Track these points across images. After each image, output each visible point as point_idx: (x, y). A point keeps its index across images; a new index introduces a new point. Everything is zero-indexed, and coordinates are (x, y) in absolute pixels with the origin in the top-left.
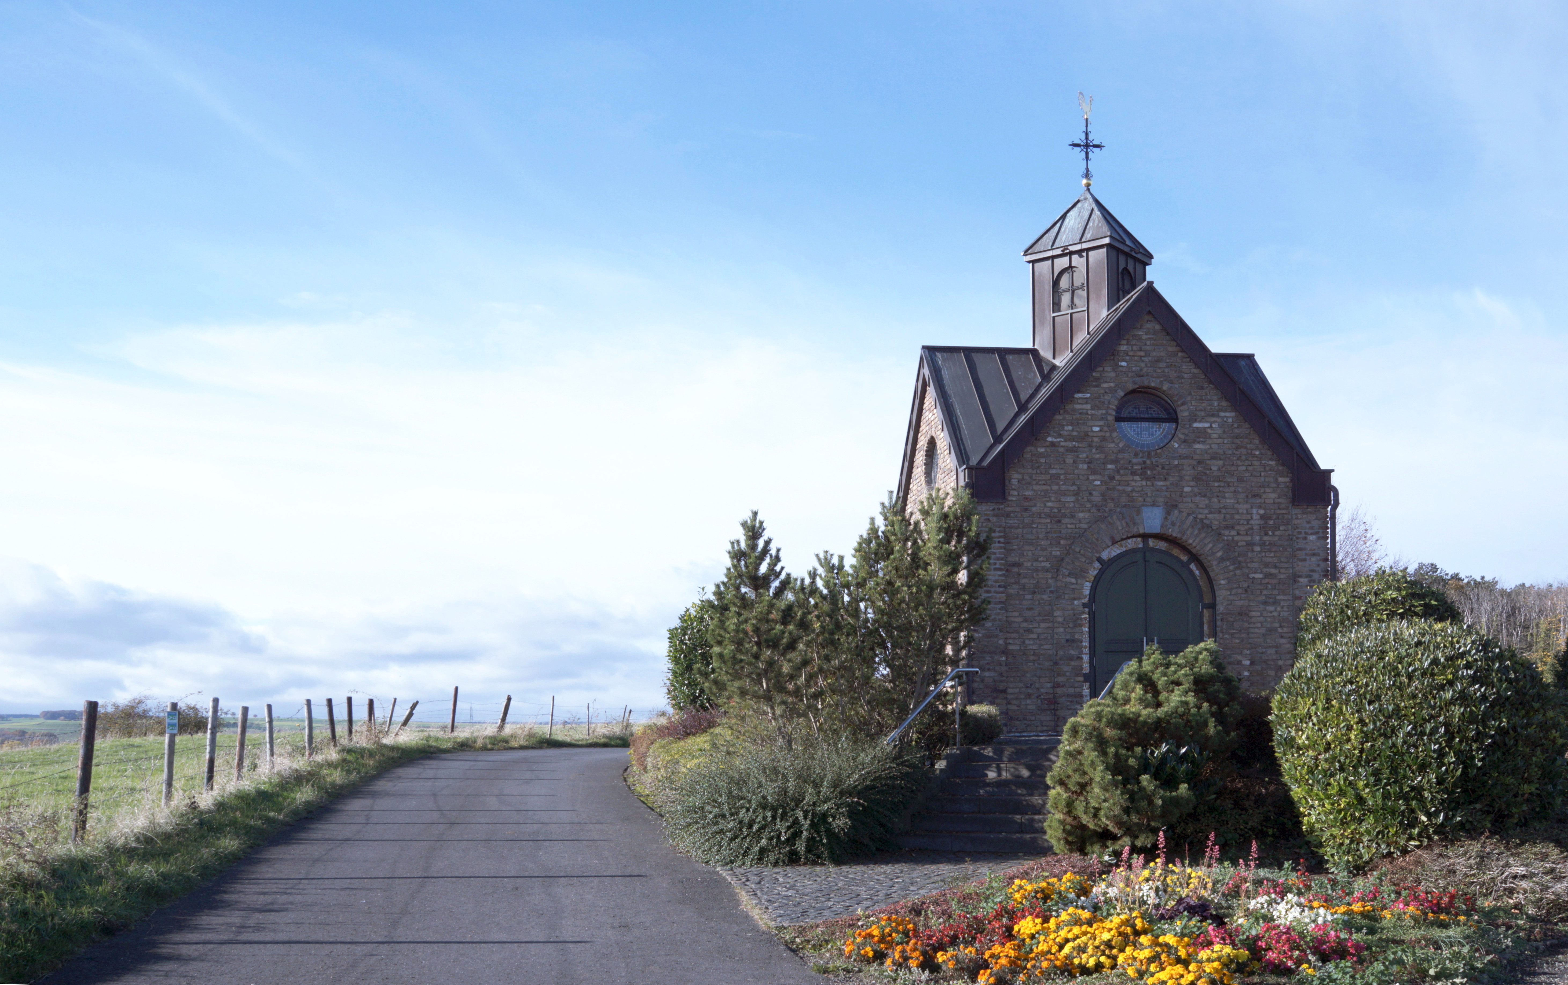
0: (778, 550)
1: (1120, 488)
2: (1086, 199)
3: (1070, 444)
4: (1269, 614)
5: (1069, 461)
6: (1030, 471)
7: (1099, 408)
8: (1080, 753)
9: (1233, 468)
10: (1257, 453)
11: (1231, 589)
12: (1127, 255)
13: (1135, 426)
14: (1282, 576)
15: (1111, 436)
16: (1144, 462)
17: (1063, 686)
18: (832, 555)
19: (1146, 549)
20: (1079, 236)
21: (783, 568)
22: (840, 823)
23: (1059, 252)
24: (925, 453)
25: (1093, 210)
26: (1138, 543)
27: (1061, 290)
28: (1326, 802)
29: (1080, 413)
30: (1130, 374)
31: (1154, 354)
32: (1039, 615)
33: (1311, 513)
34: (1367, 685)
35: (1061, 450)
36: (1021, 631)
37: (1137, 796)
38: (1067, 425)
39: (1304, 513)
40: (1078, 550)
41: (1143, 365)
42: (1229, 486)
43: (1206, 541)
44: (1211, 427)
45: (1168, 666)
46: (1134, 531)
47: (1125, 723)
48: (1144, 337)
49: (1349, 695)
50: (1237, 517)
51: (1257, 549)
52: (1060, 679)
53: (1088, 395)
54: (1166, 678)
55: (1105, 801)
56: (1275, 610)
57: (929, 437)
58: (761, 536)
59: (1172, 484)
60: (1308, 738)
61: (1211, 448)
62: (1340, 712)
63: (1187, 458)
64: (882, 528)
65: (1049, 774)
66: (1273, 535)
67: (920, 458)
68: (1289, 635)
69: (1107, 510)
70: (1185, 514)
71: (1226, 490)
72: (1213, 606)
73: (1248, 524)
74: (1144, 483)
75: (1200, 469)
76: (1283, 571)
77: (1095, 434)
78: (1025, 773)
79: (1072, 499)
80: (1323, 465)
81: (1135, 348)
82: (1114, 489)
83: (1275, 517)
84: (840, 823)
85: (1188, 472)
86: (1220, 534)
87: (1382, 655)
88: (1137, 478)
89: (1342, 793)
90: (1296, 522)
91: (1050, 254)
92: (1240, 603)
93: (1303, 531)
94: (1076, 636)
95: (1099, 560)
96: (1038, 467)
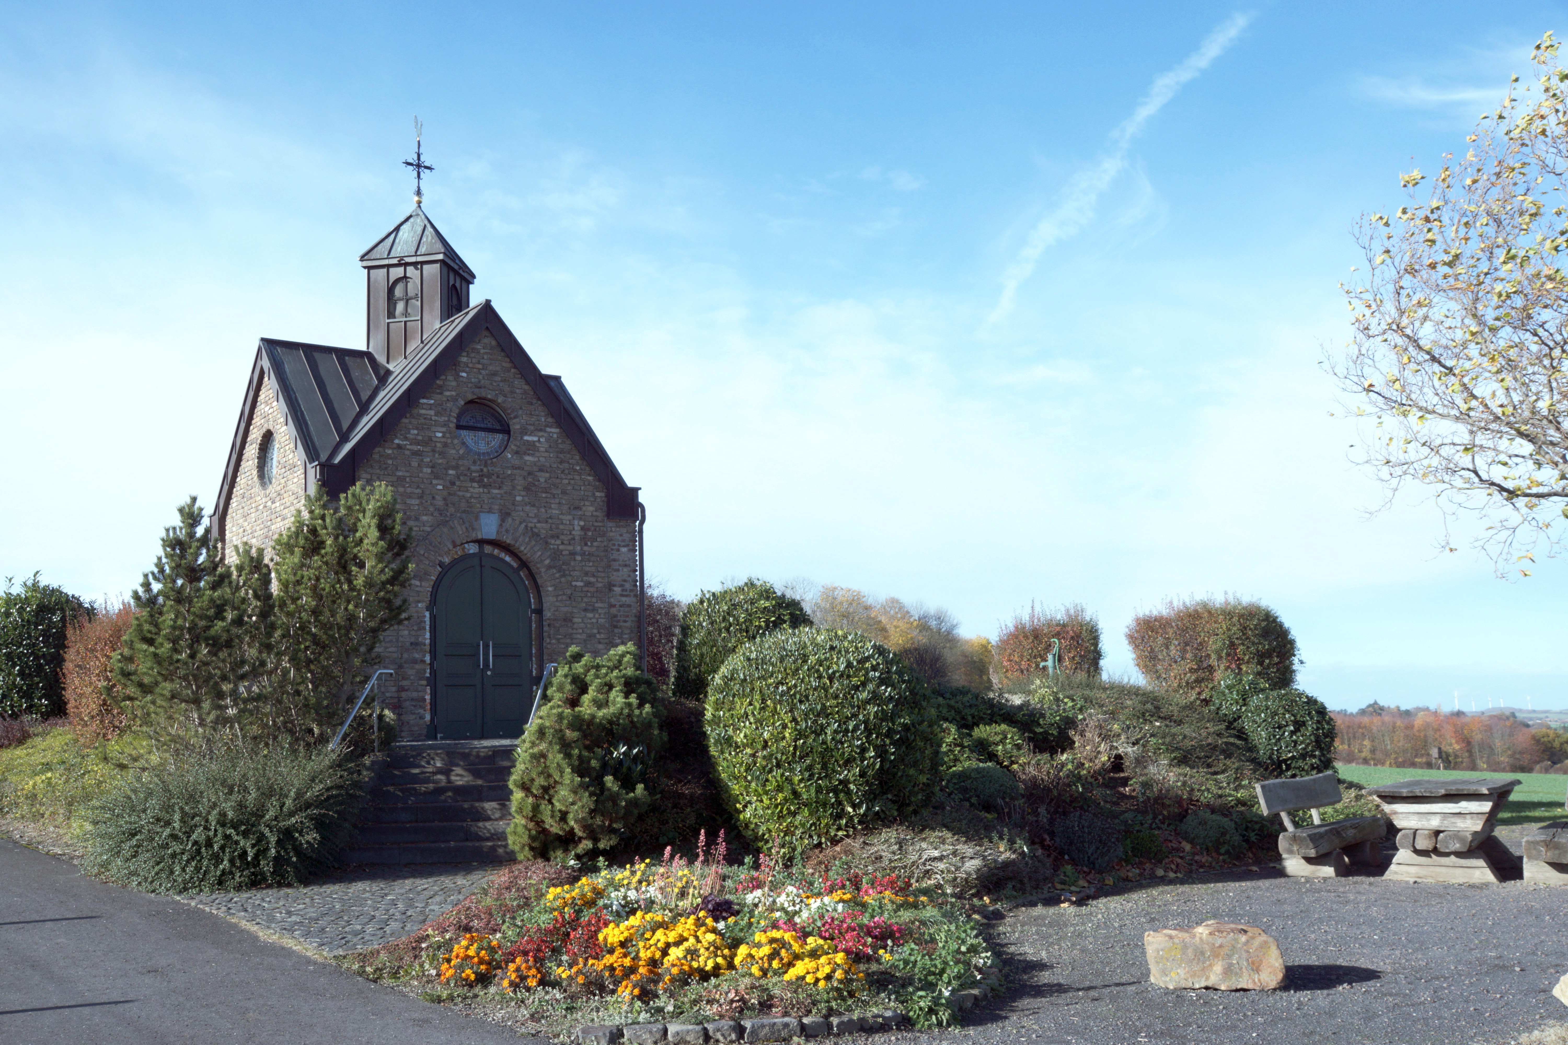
1: (461, 493)
2: (418, 215)
3: (415, 448)
5: (415, 464)
7: (442, 415)
9: (558, 481)
11: (557, 596)
12: (456, 273)
13: (472, 433)
14: (600, 585)
16: (482, 470)
19: (480, 555)
20: (414, 249)
23: (395, 261)
26: (473, 549)
28: (765, 798)
31: (491, 368)
34: (795, 686)
35: (407, 452)
39: (617, 526)
40: (422, 552)
43: (536, 549)
45: (598, 667)
46: (473, 536)
48: (482, 351)
49: (782, 696)
51: (579, 558)
52: (405, 683)
55: (573, 804)
57: (264, 430)
60: (745, 736)
62: (775, 712)
63: (519, 468)
67: (251, 451)
70: (517, 522)
72: (539, 612)
79: (417, 502)
80: (630, 483)
81: (474, 360)
82: (455, 494)
85: (520, 482)
86: (547, 543)
88: (475, 485)
89: (779, 789)
90: (612, 534)
91: (386, 262)
92: (565, 609)
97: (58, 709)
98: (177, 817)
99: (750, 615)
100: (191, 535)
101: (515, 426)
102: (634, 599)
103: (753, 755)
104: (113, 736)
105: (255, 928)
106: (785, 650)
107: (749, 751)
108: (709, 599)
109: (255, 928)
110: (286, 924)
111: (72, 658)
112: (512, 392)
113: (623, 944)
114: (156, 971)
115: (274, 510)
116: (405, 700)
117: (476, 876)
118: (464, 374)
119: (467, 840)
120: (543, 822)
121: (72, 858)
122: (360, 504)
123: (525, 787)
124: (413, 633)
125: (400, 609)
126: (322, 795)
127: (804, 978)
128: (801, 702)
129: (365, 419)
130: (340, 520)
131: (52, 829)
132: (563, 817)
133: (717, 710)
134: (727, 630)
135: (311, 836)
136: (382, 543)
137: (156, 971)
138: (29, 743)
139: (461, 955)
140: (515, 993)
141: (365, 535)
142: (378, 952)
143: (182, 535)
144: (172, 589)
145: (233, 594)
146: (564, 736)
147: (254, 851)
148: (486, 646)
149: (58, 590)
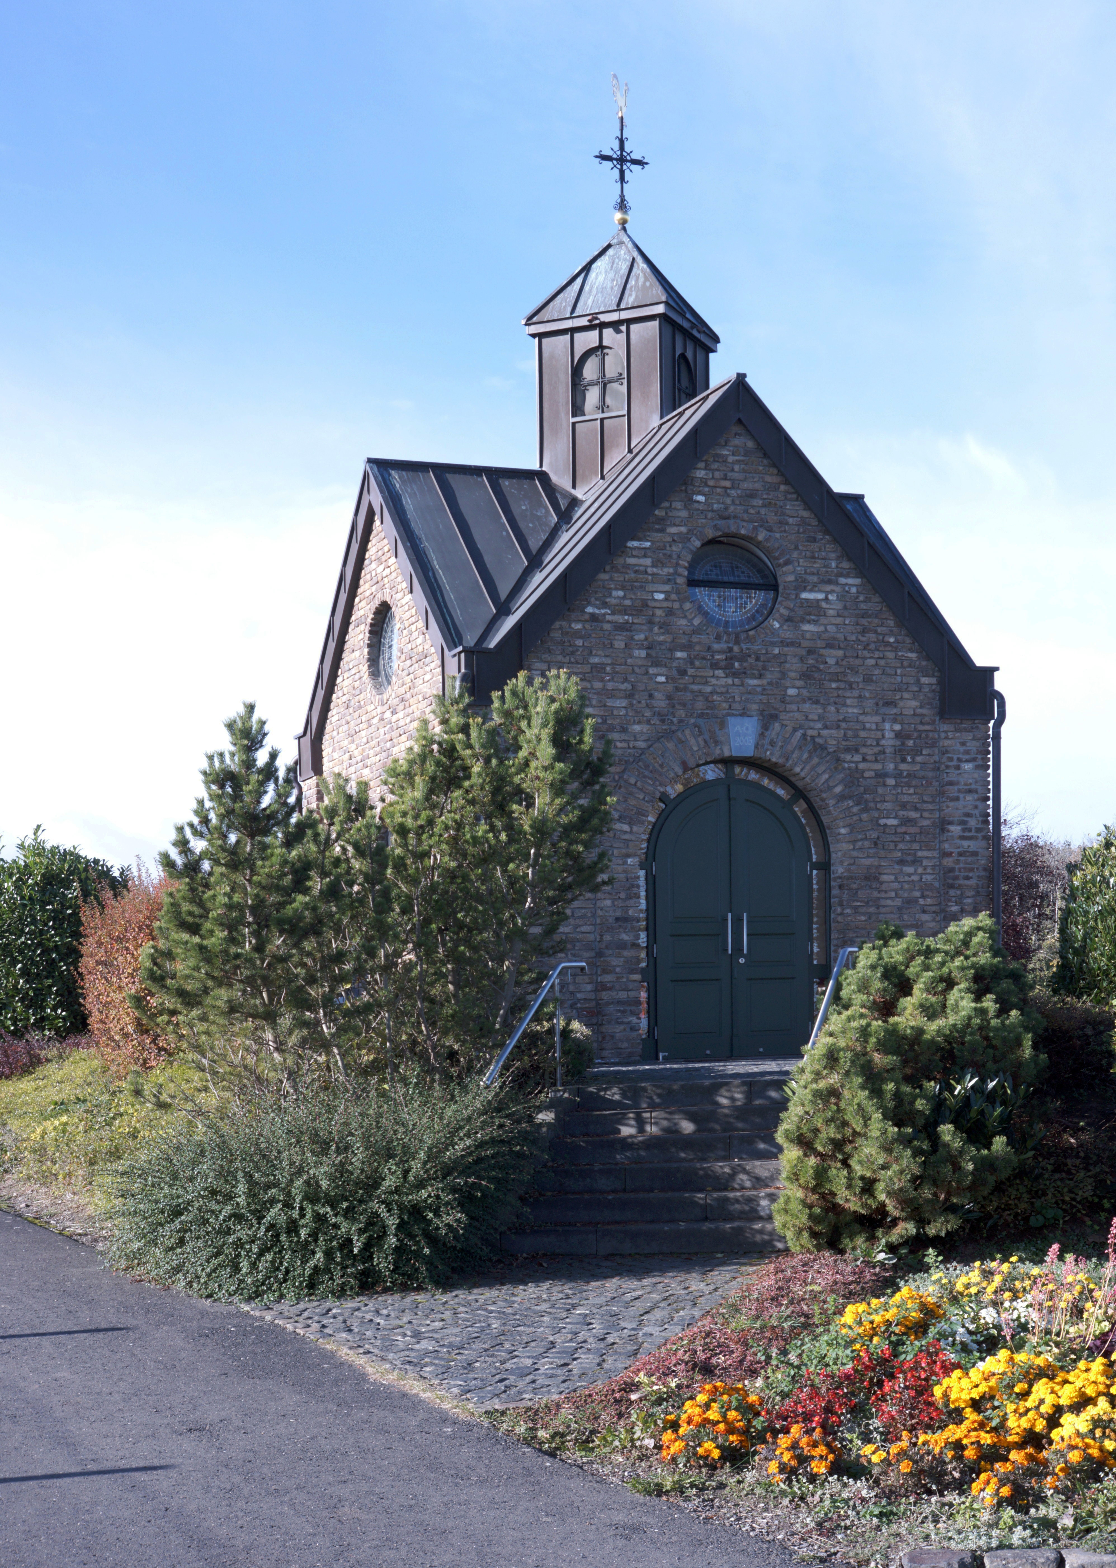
1: (695, 687)
2: (621, 243)
4: (907, 878)
5: (619, 644)
7: (664, 565)
9: (858, 662)
10: (892, 640)
14: (926, 823)
15: (681, 608)
16: (730, 650)
17: (610, 989)
19: (728, 784)
20: (615, 300)
23: (584, 322)
24: (368, 628)
25: (634, 259)
27: (585, 382)
29: (636, 572)
30: (710, 515)
31: (745, 485)
33: (966, 730)
35: (607, 626)
38: (617, 589)
39: (956, 731)
40: (632, 781)
41: (728, 501)
42: (851, 688)
43: (820, 769)
44: (826, 599)
45: (929, 953)
46: (717, 752)
48: (731, 459)
50: (863, 734)
51: (891, 782)
52: (608, 978)
53: (648, 544)
54: (930, 973)
55: (885, 1167)
56: (915, 873)
57: (377, 603)
61: (826, 630)
63: (792, 644)
66: (913, 762)
68: (934, 908)
69: (675, 720)
70: (789, 729)
71: (848, 694)
72: (825, 866)
73: (878, 744)
74: (730, 681)
75: (811, 662)
76: (926, 814)
77: (657, 605)
78: (687, 1127)
80: (980, 660)
81: (717, 475)
82: (685, 689)
83: (915, 735)
85: (794, 666)
86: (838, 760)
88: (719, 673)
90: (947, 743)
91: (569, 324)
92: (868, 862)
93: (955, 757)
94: (631, 913)
96: (573, 653)
97: (78, 1025)
98: (242, 1187)
100: (249, 764)
101: (787, 577)
102: (983, 844)
104: (158, 1063)
105: (360, 1361)
109: (360, 1361)
110: (414, 1353)
111: (91, 950)
112: (782, 523)
113: (976, 1405)
114: (202, 1430)
115: (389, 724)
116: (607, 1004)
117: (720, 1275)
118: (701, 498)
119: (706, 1219)
120: (834, 1194)
121: (96, 1240)
122: (526, 707)
123: (805, 1142)
124: (619, 903)
125: (595, 868)
126: (470, 1154)
129: (538, 577)
130: (493, 733)
131: (69, 1196)
132: (868, 1186)
135: (452, 1218)
136: (560, 766)
137: (202, 1430)
138: (40, 1071)
139: (697, 1419)
140: (790, 1486)
141: (533, 754)
142: (558, 1406)
143: (233, 764)
144: (223, 848)
145: (322, 852)
146: (870, 1062)
147: (363, 1239)
148: (737, 922)
149: (71, 854)
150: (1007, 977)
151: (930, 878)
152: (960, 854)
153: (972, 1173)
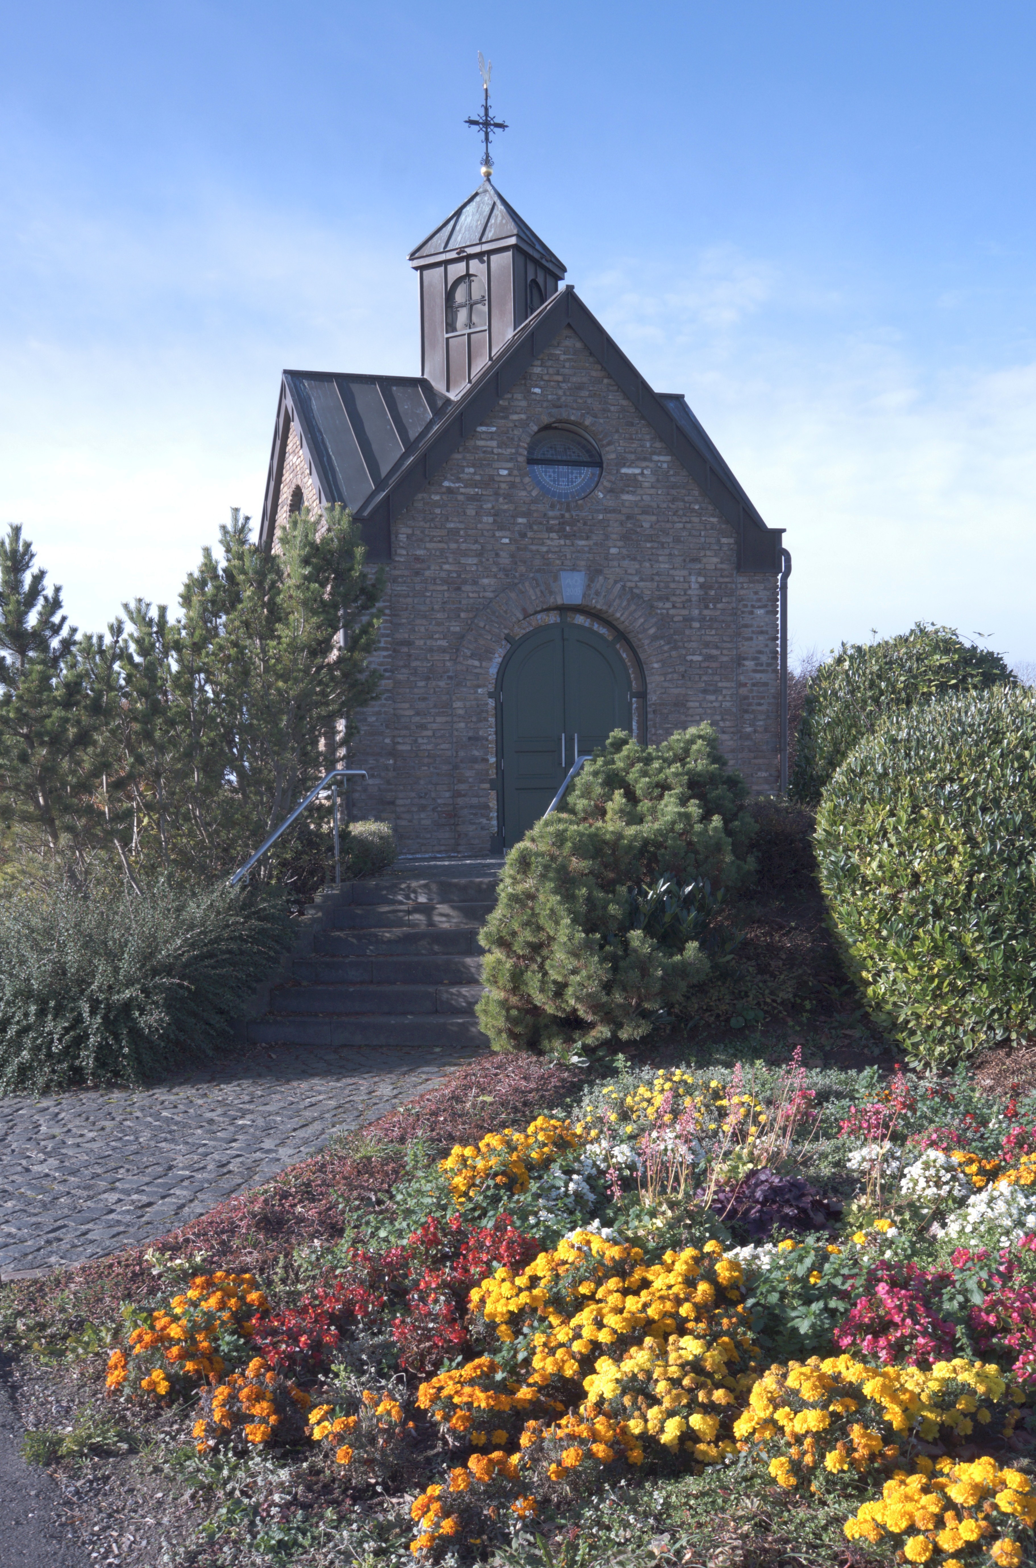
0: (58, 590)
1: (534, 548)
2: (486, 191)
3: (471, 491)
5: (471, 512)
6: (422, 524)
8: (532, 897)
9: (669, 525)
11: (665, 675)
12: (537, 263)
14: (725, 659)
16: (563, 516)
18: (148, 605)
20: (478, 236)
21: (64, 619)
22: (152, 1019)
23: (453, 255)
26: (553, 618)
28: (910, 966)
31: (574, 379)
32: (435, 706)
34: (976, 783)
35: (461, 498)
36: (413, 727)
37: (622, 964)
39: (750, 582)
40: (482, 624)
41: (560, 392)
43: (638, 614)
44: (642, 474)
45: (648, 760)
46: (551, 601)
47: (595, 847)
48: (562, 357)
49: (950, 798)
50: (672, 585)
51: (696, 625)
52: (462, 787)
55: (574, 972)
58: (27, 566)
59: (596, 544)
60: (881, 866)
63: (614, 511)
64: (223, 564)
65: (483, 931)
66: (715, 608)
70: (611, 581)
71: (660, 552)
72: (642, 695)
74: (562, 542)
80: (771, 523)
81: (551, 371)
84: (152, 1019)
86: (652, 607)
87: (997, 737)
88: (554, 535)
89: (937, 951)
90: (742, 592)
91: (443, 257)
92: (676, 691)
95: (508, 638)
96: (433, 520)
99: (915, 677)
101: (609, 455)
102: (773, 676)
103: (894, 897)
106: (960, 722)
107: (885, 889)
108: (851, 657)
118: (537, 390)
127: (897, 1541)
128: (984, 810)
132: (560, 989)
133: (834, 823)
134: (876, 701)
150: (724, 783)
151: (728, 704)
152: (754, 685)
153: (662, 978)
